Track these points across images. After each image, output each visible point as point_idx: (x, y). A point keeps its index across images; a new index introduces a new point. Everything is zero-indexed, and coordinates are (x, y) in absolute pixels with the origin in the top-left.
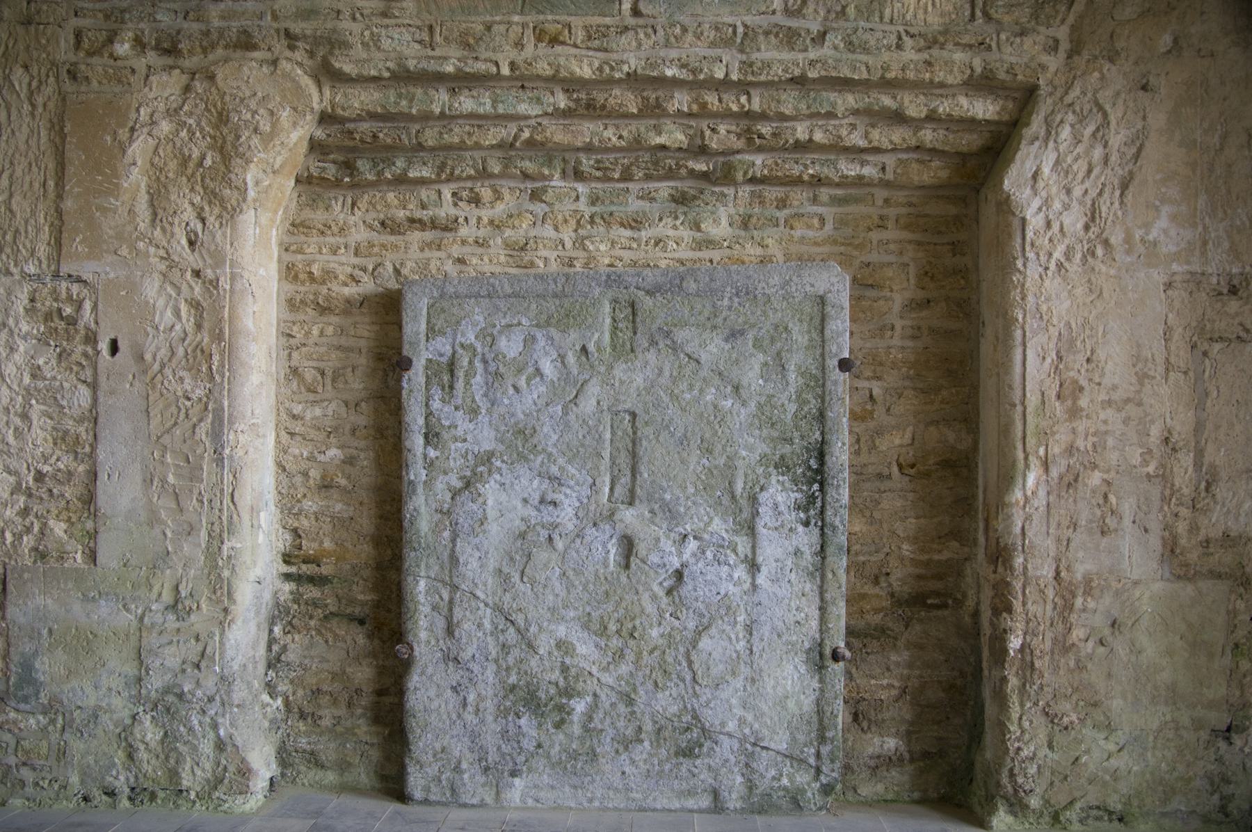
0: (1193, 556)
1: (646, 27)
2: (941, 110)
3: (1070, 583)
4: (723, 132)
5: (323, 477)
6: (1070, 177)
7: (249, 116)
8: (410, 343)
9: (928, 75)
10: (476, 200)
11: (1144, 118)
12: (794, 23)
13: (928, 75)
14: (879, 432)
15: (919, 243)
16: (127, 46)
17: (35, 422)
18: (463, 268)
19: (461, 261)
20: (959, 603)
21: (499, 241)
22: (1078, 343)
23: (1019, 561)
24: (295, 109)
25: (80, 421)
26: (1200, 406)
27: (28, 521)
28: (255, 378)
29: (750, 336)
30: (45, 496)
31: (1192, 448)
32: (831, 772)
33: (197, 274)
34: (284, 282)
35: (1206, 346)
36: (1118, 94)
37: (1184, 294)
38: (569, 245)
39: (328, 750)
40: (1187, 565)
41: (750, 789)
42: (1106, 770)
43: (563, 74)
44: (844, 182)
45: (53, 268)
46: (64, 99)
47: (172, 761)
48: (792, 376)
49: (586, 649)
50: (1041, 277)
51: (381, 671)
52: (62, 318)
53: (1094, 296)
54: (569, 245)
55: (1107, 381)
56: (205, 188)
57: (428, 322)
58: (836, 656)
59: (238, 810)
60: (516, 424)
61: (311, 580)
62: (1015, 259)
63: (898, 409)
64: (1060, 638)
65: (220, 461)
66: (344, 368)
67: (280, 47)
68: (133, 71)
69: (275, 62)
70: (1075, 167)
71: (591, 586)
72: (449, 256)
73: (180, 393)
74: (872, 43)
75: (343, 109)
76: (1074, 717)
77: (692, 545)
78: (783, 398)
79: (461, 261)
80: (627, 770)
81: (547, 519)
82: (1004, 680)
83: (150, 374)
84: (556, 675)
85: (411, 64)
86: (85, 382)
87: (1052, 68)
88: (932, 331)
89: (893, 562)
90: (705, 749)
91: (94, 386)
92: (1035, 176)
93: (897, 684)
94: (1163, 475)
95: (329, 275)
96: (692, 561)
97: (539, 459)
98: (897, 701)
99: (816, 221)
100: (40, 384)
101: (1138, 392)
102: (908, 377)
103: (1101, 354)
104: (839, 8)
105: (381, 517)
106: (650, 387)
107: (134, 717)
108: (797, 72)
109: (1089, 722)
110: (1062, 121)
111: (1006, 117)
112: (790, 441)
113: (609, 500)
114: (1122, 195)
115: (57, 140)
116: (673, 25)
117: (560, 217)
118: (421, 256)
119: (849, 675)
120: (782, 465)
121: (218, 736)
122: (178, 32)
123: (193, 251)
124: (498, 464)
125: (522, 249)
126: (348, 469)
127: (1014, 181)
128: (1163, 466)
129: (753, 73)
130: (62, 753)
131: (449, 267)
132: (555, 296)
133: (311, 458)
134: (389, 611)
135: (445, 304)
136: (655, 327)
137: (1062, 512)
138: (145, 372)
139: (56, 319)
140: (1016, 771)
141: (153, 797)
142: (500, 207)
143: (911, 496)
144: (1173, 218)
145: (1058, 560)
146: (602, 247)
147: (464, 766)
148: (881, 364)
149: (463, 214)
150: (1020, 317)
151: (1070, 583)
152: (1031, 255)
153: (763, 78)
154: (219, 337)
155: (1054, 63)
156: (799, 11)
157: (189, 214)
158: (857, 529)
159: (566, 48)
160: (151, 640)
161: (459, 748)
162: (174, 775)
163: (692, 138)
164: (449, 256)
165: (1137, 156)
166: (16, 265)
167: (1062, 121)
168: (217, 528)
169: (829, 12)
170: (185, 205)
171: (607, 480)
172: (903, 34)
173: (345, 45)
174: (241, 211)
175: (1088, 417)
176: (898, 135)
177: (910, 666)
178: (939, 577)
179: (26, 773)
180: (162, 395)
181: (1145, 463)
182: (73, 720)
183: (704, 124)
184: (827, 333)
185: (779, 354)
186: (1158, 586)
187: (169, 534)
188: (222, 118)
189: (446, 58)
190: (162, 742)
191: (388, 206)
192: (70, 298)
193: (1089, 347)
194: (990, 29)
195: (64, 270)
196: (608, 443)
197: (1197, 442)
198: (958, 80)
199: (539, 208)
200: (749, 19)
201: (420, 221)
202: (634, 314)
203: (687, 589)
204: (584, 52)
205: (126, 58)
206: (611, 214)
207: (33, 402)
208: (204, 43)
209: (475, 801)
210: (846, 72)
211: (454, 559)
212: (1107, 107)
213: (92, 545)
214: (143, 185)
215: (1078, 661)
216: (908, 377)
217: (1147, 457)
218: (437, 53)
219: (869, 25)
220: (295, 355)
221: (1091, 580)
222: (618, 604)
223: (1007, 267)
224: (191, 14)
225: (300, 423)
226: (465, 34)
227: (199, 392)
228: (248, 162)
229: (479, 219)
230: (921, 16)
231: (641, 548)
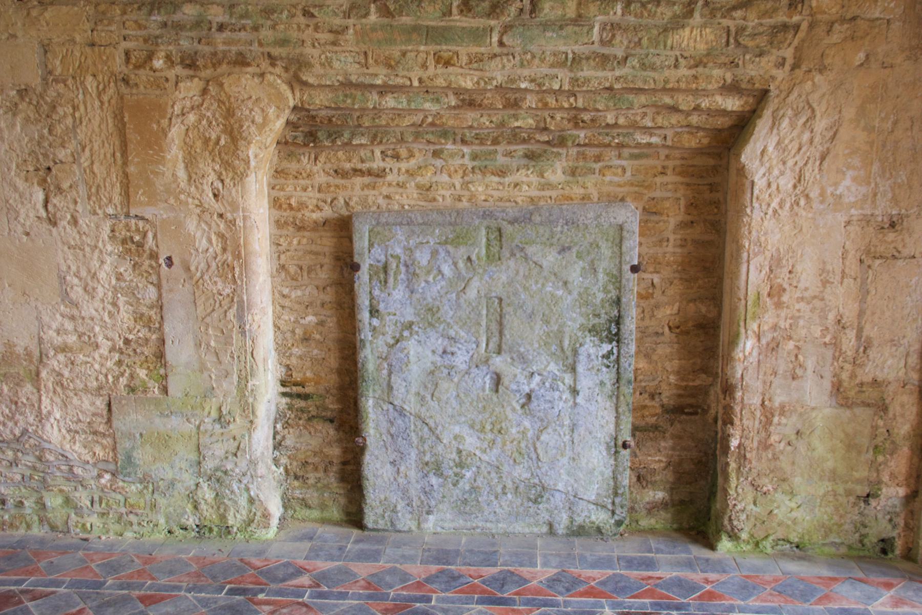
0: (852, 394)
1: (507, 55)
2: (703, 105)
3: (771, 408)
4: (559, 118)
5: (305, 333)
6: (786, 153)
7: (247, 112)
8: (359, 254)
9: (694, 85)
10: (397, 157)
11: (840, 112)
12: (606, 51)
13: (694, 85)
14: (657, 306)
15: (688, 185)
16: (161, 62)
17: (121, 308)
18: (389, 201)
19: (388, 197)
20: (706, 412)
21: (413, 184)
22: (784, 262)
23: (738, 394)
24: (278, 108)
25: (151, 307)
26: (863, 301)
27: (122, 369)
28: (261, 279)
29: (574, 250)
30: (131, 353)
31: (855, 327)
32: (621, 513)
33: (221, 216)
34: (272, 210)
35: (870, 262)
36: (824, 95)
37: (857, 228)
38: (458, 186)
39: (313, 496)
40: (847, 398)
41: (572, 522)
42: (789, 519)
43: (453, 86)
44: (638, 145)
45: (125, 210)
46: (122, 98)
47: (222, 510)
48: (601, 276)
49: (471, 442)
50: (762, 219)
51: (345, 451)
52: (133, 242)
53: (796, 231)
54: (458, 186)
55: (801, 285)
56: (222, 160)
57: (370, 241)
58: (625, 446)
59: (264, 538)
60: (427, 305)
61: (299, 396)
62: (746, 207)
63: (670, 292)
64: (763, 441)
65: (243, 333)
66: (315, 265)
67: (265, 65)
68: (167, 80)
69: (262, 75)
70: (790, 147)
71: (475, 403)
72: (381, 194)
73: (215, 291)
74: (658, 63)
75: (309, 105)
76: (770, 487)
77: (537, 379)
78: (595, 289)
79: (388, 197)
80: (497, 510)
81: (447, 362)
82: (727, 464)
83: (195, 279)
84: (454, 455)
85: (354, 78)
86: (152, 283)
87: (780, 79)
88: (694, 241)
89: (664, 386)
90: (544, 499)
91: (159, 286)
92: (763, 152)
93: (664, 460)
94: (835, 344)
95: (302, 205)
96: (537, 388)
97: (442, 327)
98: (664, 470)
99: (620, 170)
100: (123, 284)
101: (822, 292)
102: (677, 271)
103: (799, 268)
104: (636, 40)
105: (343, 358)
106: (510, 283)
107: (197, 485)
108: (607, 85)
109: (780, 490)
110: (783, 116)
111: (747, 108)
112: (598, 316)
113: (486, 351)
114: (821, 164)
115: (120, 125)
116: (525, 53)
117: (452, 169)
118: (362, 193)
119: (634, 455)
120: (593, 330)
121: (250, 495)
122: (196, 53)
123: (217, 201)
124: (417, 329)
125: (427, 190)
126: (320, 328)
127: (749, 156)
128: (835, 338)
129: (578, 85)
130: (154, 506)
131: (380, 201)
132: (450, 224)
133: (296, 322)
134: (349, 414)
135: (379, 229)
136: (514, 245)
137: (768, 365)
138: (191, 278)
139: (129, 243)
140: (733, 518)
142: (413, 162)
143: (676, 346)
144: (854, 179)
145: (764, 394)
146: (480, 189)
147: (399, 508)
148: (659, 263)
149: (389, 166)
150: (747, 245)
151: (771, 408)
152: (756, 205)
153: (584, 89)
154: (238, 256)
155: (780, 74)
156: (610, 41)
157: (212, 177)
158: (641, 366)
159: (455, 68)
160: (205, 440)
162: (223, 517)
163: (538, 122)
164: (381, 194)
165: (833, 138)
166: (100, 208)
167: (783, 116)
168: (243, 373)
169: (630, 42)
170: (209, 170)
171: (484, 339)
172: (679, 57)
173: (309, 65)
174: (247, 176)
175: (788, 307)
176: (674, 119)
177: (673, 449)
178: (692, 396)
179: (132, 517)
180: (203, 292)
181: (824, 336)
182: (159, 487)
183: (546, 114)
184: (624, 249)
185: (592, 261)
186: (827, 411)
187: (213, 377)
188: (230, 113)
189: (376, 75)
190: (215, 499)
191: (338, 160)
192: (138, 230)
193: (790, 264)
194: (739, 51)
195: (133, 212)
196: (484, 317)
197: (859, 323)
198: (716, 86)
199: (439, 163)
200: (576, 48)
201: (360, 170)
202: (501, 236)
203: (534, 404)
204: (467, 71)
205: (161, 70)
206: (486, 167)
207: (119, 295)
208: (214, 61)
209: (406, 529)
210: (640, 85)
211: (390, 388)
212: (815, 105)
213: (164, 383)
214: (180, 156)
215: (774, 455)
216: (677, 271)
217: (825, 332)
218: (371, 71)
219: (657, 52)
220: (283, 257)
221: (784, 407)
222: (491, 414)
223: (740, 212)
224: (203, 40)
225: (288, 300)
226: (388, 58)
227: (228, 291)
228: (249, 143)
229: (399, 169)
230: (692, 44)
231: (506, 381)
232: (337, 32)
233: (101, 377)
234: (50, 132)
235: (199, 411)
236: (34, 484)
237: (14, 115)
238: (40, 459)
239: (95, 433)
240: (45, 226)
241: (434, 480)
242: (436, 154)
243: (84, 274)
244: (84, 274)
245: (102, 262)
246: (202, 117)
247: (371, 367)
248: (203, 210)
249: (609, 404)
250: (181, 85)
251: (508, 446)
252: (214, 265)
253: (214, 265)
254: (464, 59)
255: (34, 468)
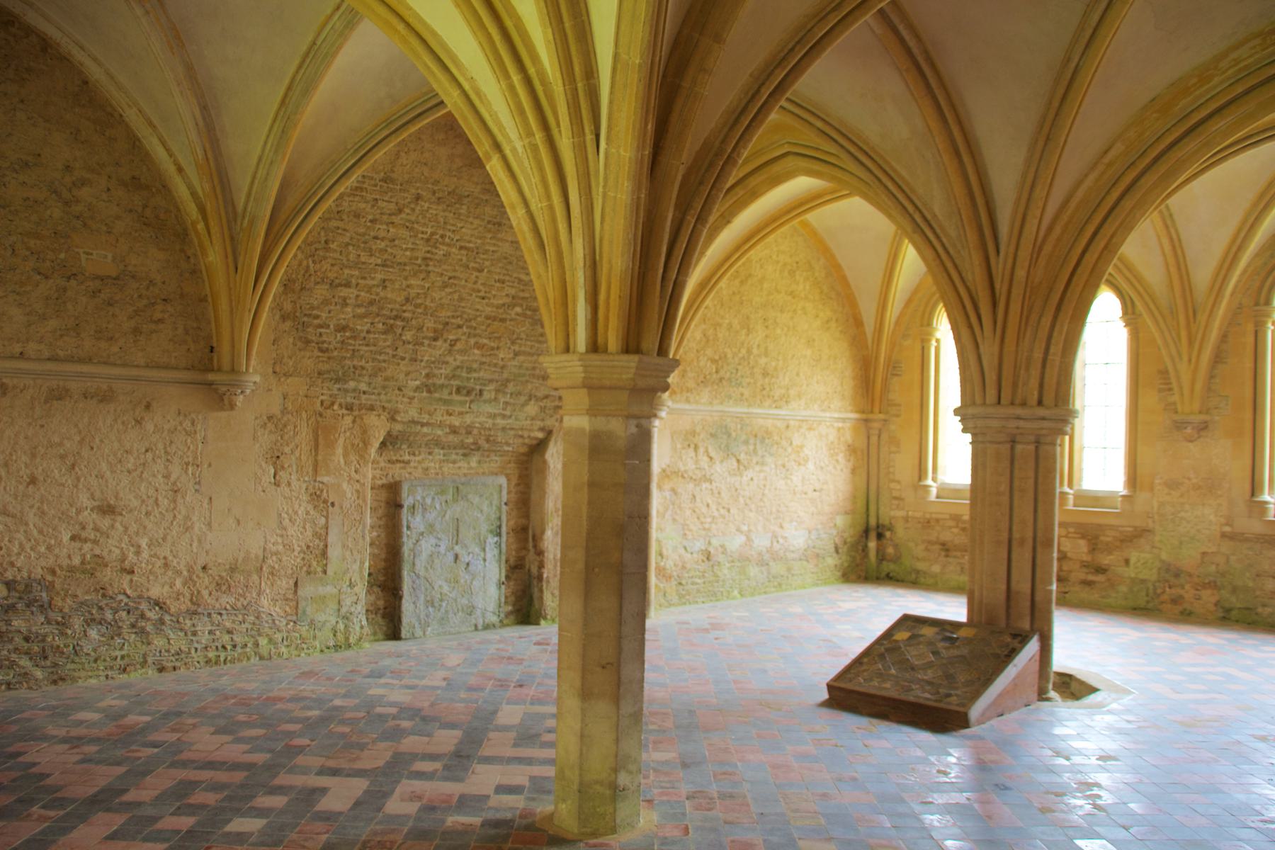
10: (414, 454)
12: (503, 412)
19: (410, 473)
23: (546, 554)
49: (446, 588)
58: (503, 583)
77: (471, 555)
79: (410, 473)
82: (542, 586)
84: (439, 596)
85: (416, 419)
91: (327, 518)
100: (309, 517)
120: (491, 532)
130: (315, 637)
131: (407, 475)
141: (341, 647)
160: (343, 597)
161: (414, 621)
170: (353, 457)
179: (304, 646)
188: (365, 432)
192: (319, 489)
195: (318, 479)
199: (431, 457)
203: (470, 568)
211: (414, 564)
223: (544, 478)
231: (460, 556)
232: (412, 398)
233: (294, 568)
234: (282, 438)
235: (340, 582)
236: (253, 633)
237: (265, 429)
238: (257, 618)
239: (287, 600)
240: (274, 487)
241: (431, 609)
242: (430, 453)
243: (290, 511)
244: (290, 511)
245: (300, 505)
246: (352, 433)
247: (406, 555)
248: (350, 478)
249: (497, 565)
250: (345, 418)
251: (460, 589)
252: (353, 505)
253: (353, 505)
254: (457, 413)
255: (254, 624)
